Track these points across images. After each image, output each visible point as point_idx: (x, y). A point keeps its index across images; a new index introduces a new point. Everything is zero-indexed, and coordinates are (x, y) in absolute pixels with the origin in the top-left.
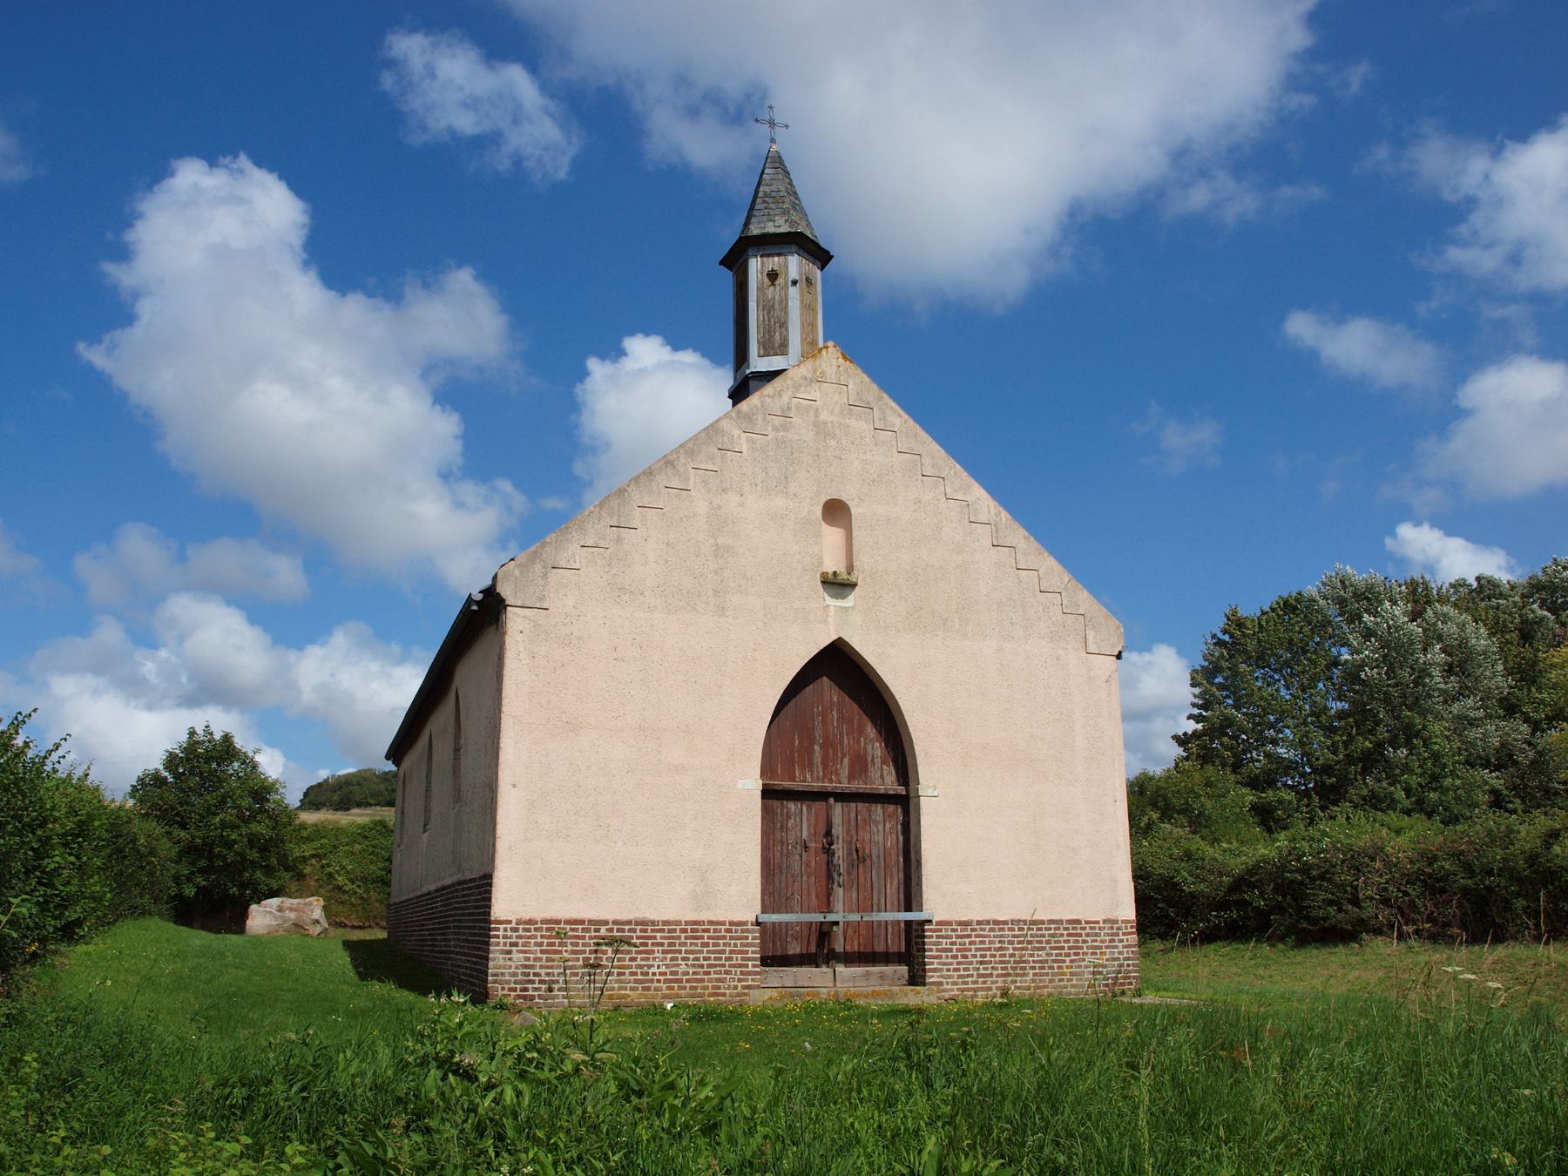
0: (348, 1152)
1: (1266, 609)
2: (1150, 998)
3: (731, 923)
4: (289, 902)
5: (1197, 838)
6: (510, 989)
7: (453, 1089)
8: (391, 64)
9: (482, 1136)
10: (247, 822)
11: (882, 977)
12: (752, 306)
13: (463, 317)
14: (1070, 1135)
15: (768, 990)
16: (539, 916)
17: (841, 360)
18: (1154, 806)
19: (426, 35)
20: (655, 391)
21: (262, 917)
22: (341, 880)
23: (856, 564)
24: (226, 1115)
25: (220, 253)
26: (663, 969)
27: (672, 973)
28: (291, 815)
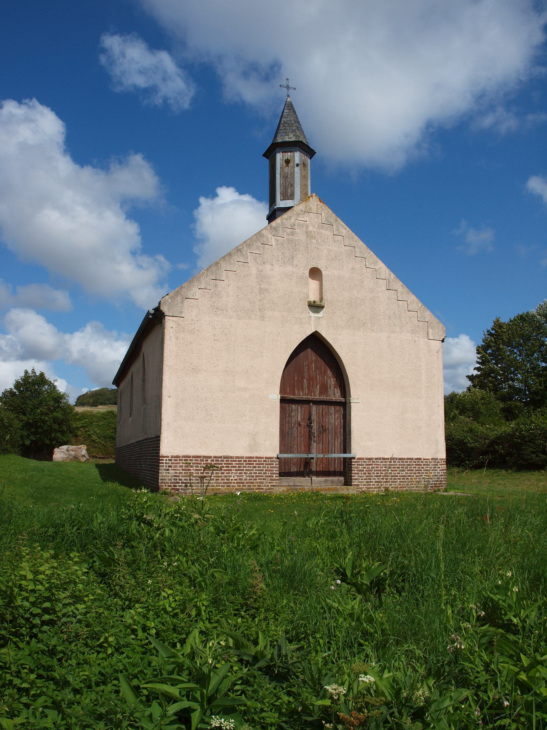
0: (98, 556)
1: (512, 319)
2: (452, 493)
3: (266, 458)
4: (71, 447)
5: (475, 422)
6: (169, 486)
7: (143, 530)
8: (104, 51)
9: (155, 550)
10: (52, 411)
11: (333, 482)
12: (278, 176)
13: (138, 178)
14: (410, 552)
15: (282, 487)
16: (181, 454)
17: (319, 202)
18: (457, 408)
19: (121, 37)
20: (231, 214)
21: (60, 454)
22: (94, 437)
23: (324, 297)
24: (45, 540)
25: (24, 147)
26: (236, 478)
27: (240, 479)
28: (71, 408)
